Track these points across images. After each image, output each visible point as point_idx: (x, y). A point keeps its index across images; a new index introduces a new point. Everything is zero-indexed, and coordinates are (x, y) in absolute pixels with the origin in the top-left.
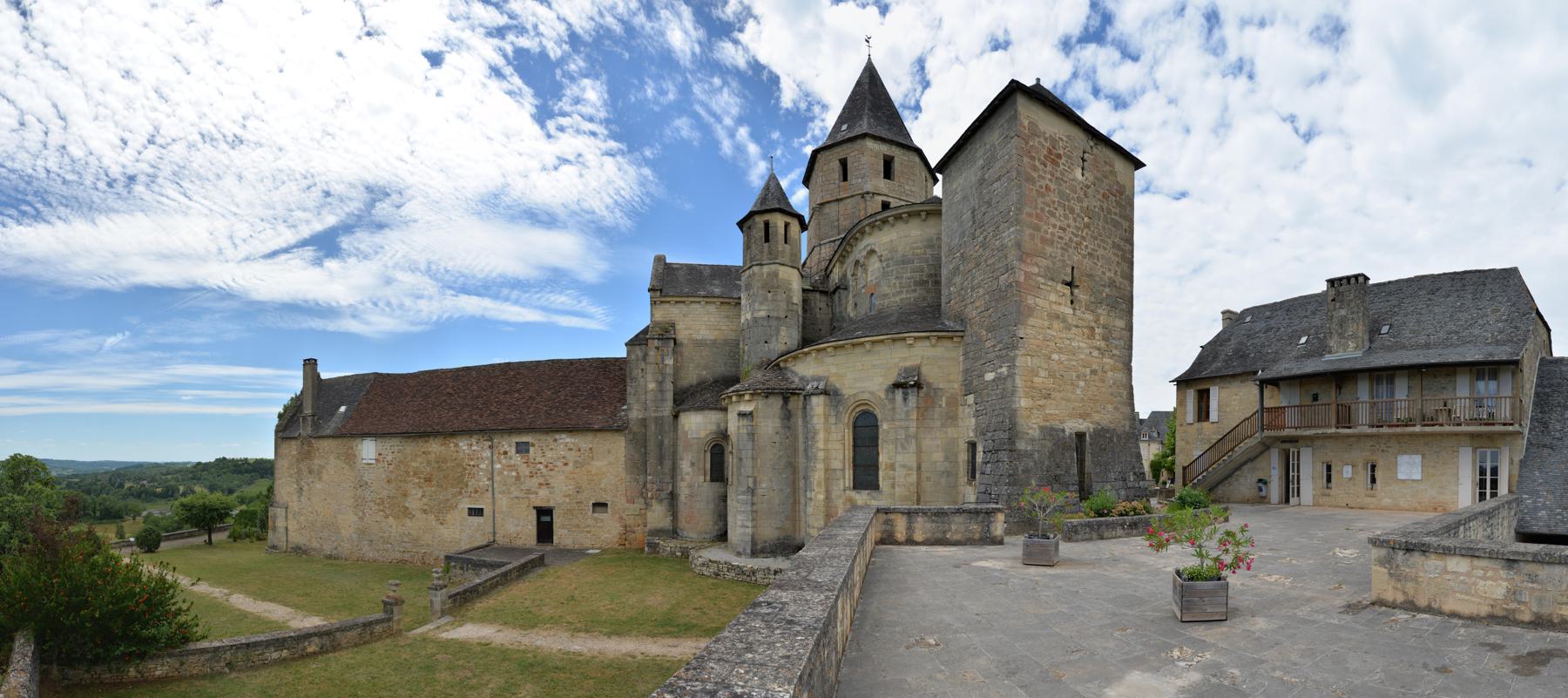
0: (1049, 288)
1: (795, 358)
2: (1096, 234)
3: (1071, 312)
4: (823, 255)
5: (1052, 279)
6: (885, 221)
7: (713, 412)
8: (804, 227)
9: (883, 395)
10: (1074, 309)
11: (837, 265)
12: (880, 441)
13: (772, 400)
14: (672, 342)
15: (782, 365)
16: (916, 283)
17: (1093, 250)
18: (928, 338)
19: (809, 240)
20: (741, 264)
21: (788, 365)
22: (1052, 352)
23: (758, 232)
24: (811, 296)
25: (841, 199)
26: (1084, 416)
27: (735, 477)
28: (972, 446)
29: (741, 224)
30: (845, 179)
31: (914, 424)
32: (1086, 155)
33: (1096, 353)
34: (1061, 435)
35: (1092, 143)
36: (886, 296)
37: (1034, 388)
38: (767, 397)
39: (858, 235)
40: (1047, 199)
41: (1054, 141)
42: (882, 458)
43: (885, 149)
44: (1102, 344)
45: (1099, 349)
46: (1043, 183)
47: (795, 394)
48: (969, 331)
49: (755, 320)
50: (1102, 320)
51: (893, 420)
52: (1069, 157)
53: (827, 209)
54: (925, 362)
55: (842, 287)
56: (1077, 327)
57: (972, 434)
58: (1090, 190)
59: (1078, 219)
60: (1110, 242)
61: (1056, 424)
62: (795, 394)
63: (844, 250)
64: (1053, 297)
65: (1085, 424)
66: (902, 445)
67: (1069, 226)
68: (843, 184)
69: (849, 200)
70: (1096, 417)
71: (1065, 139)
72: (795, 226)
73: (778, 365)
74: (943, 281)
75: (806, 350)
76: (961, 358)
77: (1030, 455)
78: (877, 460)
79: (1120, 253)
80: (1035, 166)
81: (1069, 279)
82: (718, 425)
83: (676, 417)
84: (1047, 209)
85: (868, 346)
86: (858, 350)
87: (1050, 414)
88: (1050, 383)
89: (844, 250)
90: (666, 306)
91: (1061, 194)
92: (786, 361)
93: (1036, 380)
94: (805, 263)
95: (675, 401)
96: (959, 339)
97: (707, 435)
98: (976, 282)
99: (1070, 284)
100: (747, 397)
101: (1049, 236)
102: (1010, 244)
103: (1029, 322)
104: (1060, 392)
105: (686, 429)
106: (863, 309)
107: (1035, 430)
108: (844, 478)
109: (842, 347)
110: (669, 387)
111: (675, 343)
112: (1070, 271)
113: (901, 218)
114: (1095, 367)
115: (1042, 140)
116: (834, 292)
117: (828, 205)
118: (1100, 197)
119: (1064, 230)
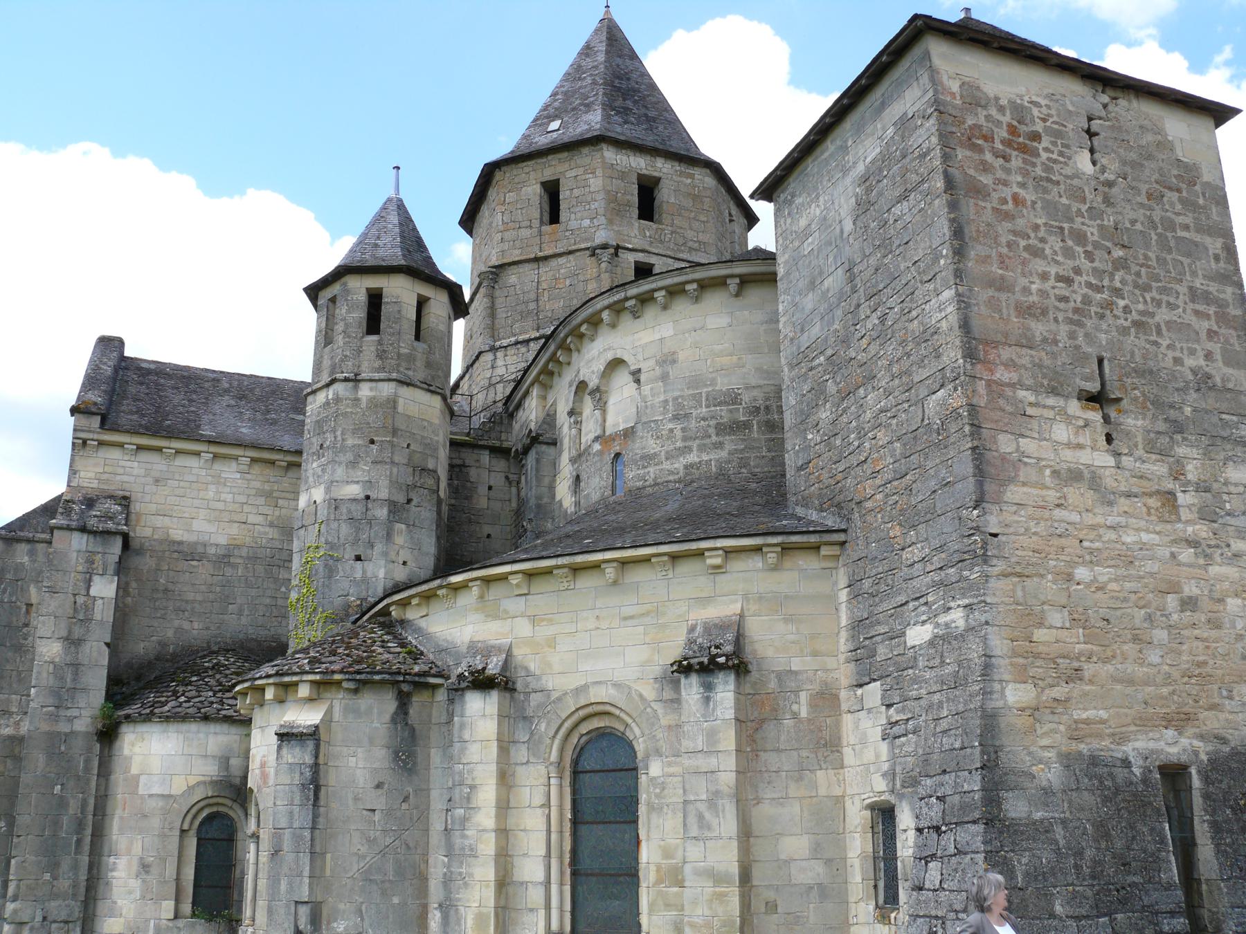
0: (1051, 414)
1: (428, 597)
2: (1144, 279)
3: (1111, 461)
4: (501, 371)
5: (1054, 391)
6: (645, 300)
7: (213, 727)
8: (459, 308)
9: (649, 692)
10: (1117, 454)
11: (535, 392)
12: (642, 809)
13: (367, 700)
14: (118, 543)
15: (395, 613)
16: (721, 429)
17: (1141, 313)
18: (758, 549)
19: (469, 338)
20: (309, 380)
21: (411, 614)
22: (1072, 564)
23: (353, 312)
24: (469, 456)
25: (546, 258)
26: (1180, 720)
27: (262, 904)
28: (884, 815)
29: (313, 292)
30: (554, 217)
31: (730, 763)
32: (1096, 125)
33: (1186, 554)
34: (1121, 773)
35: (1105, 98)
36: (649, 458)
37: (1037, 656)
38: (356, 691)
39: (583, 329)
40: (1021, 223)
41: (1020, 112)
42: (648, 855)
43: (640, 163)
44: (1201, 530)
45: (1193, 543)
46: (1007, 193)
47: (427, 686)
48: (857, 531)
49: (335, 504)
50: (1192, 471)
51: (677, 755)
52: (1058, 134)
53: (512, 277)
54: (753, 607)
55: (543, 438)
56: (1129, 495)
57: (881, 785)
58: (1115, 190)
59: (1098, 254)
60: (1182, 289)
61: (1101, 746)
62: (427, 686)
63: (553, 358)
64: (1061, 432)
65: (1184, 741)
66: (701, 817)
67: (1078, 271)
68: (547, 229)
69: (562, 260)
70: (1212, 722)
71: (1043, 102)
72: (439, 303)
73: (385, 612)
74: (789, 419)
75: (455, 579)
76: (843, 595)
77: (1043, 829)
78: (636, 859)
79: (1212, 310)
80: (984, 163)
81: (1094, 387)
82: (225, 761)
83: (108, 735)
84: (1023, 243)
85: (610, 571)
86: (587, 582)
87: (1087, 722)
88: (1076, 641)
89: (553, 358)
90: (115, 454)
91: (1051, 208)
92: (405, 604)
93: (1040, 634)
94: (457, 385)
95: (109, 696)
96: (835, 550)
97: (191, 789)
98: (869, 415)
99: (1097, 399)
100: (304, 691)
101: (1034, 298)
102: (944, 324)
103: (1008, 496)
104: (1106, 661)
105: (134, 770)
106: (596, 486)
107: (1047, 763)
108: (548, 907)
109: (548, 572)
110: (96, 655)
111: (126, 545)
112: (1095, 367)
113: (684, 291)
114: (1191, 589)
115: (993, 112)
116: (526, 450)
117: (514, 269)
118: (1142, 199)
119: (1068, 281)
